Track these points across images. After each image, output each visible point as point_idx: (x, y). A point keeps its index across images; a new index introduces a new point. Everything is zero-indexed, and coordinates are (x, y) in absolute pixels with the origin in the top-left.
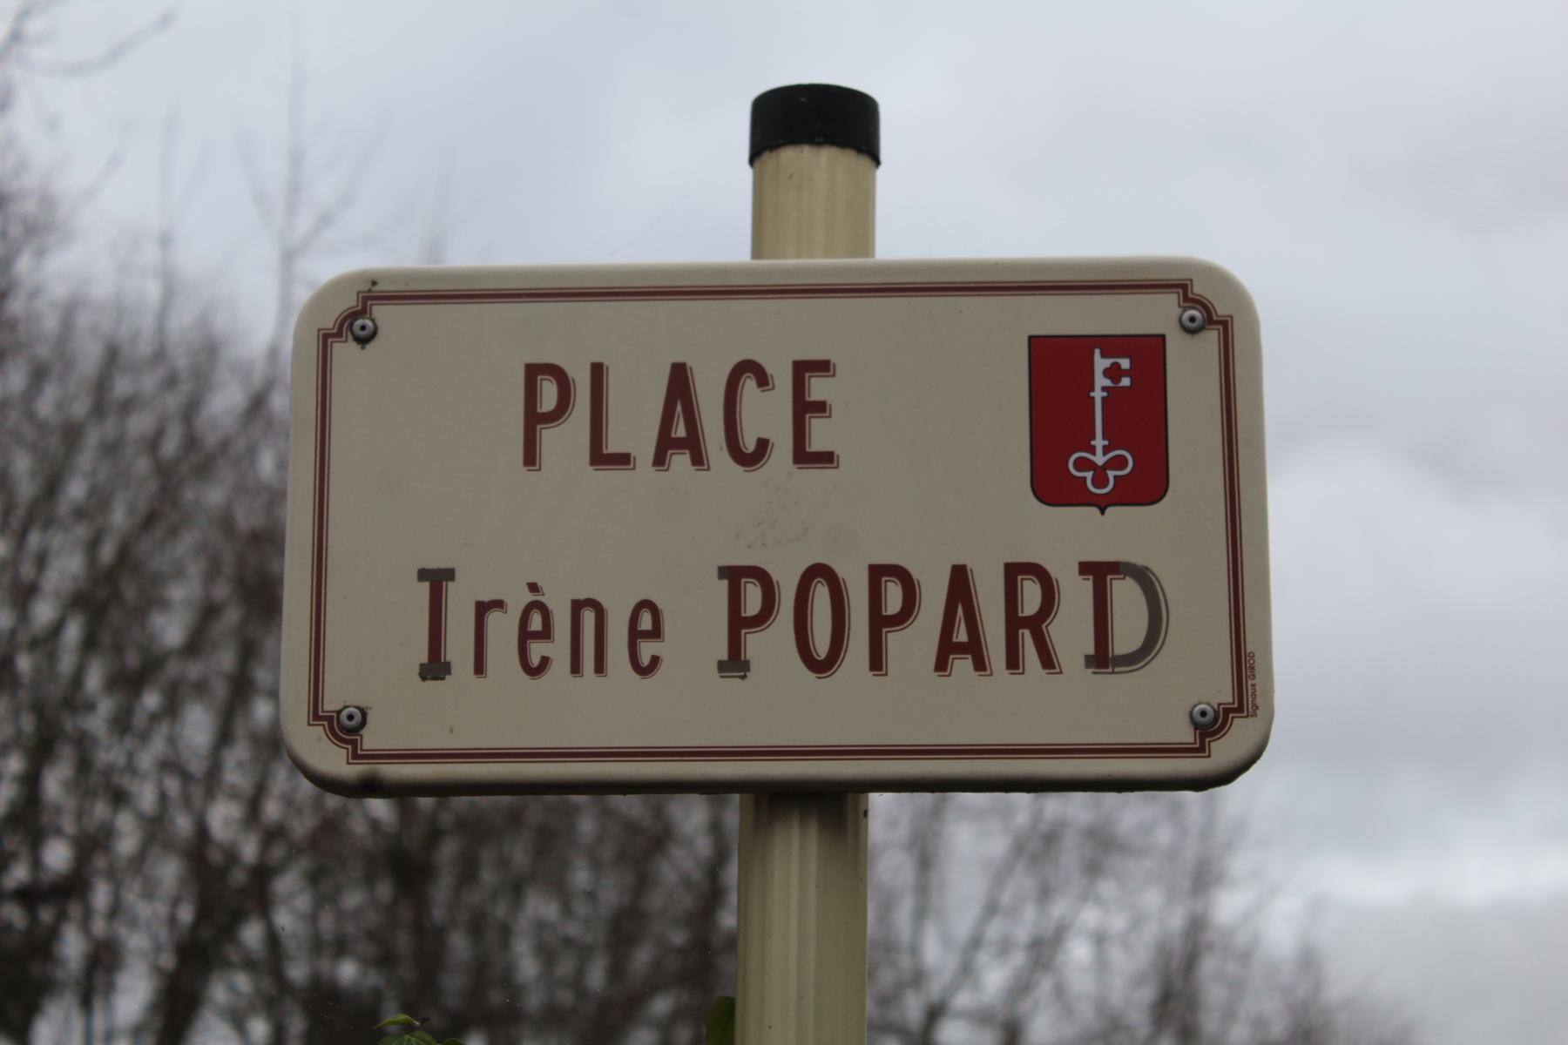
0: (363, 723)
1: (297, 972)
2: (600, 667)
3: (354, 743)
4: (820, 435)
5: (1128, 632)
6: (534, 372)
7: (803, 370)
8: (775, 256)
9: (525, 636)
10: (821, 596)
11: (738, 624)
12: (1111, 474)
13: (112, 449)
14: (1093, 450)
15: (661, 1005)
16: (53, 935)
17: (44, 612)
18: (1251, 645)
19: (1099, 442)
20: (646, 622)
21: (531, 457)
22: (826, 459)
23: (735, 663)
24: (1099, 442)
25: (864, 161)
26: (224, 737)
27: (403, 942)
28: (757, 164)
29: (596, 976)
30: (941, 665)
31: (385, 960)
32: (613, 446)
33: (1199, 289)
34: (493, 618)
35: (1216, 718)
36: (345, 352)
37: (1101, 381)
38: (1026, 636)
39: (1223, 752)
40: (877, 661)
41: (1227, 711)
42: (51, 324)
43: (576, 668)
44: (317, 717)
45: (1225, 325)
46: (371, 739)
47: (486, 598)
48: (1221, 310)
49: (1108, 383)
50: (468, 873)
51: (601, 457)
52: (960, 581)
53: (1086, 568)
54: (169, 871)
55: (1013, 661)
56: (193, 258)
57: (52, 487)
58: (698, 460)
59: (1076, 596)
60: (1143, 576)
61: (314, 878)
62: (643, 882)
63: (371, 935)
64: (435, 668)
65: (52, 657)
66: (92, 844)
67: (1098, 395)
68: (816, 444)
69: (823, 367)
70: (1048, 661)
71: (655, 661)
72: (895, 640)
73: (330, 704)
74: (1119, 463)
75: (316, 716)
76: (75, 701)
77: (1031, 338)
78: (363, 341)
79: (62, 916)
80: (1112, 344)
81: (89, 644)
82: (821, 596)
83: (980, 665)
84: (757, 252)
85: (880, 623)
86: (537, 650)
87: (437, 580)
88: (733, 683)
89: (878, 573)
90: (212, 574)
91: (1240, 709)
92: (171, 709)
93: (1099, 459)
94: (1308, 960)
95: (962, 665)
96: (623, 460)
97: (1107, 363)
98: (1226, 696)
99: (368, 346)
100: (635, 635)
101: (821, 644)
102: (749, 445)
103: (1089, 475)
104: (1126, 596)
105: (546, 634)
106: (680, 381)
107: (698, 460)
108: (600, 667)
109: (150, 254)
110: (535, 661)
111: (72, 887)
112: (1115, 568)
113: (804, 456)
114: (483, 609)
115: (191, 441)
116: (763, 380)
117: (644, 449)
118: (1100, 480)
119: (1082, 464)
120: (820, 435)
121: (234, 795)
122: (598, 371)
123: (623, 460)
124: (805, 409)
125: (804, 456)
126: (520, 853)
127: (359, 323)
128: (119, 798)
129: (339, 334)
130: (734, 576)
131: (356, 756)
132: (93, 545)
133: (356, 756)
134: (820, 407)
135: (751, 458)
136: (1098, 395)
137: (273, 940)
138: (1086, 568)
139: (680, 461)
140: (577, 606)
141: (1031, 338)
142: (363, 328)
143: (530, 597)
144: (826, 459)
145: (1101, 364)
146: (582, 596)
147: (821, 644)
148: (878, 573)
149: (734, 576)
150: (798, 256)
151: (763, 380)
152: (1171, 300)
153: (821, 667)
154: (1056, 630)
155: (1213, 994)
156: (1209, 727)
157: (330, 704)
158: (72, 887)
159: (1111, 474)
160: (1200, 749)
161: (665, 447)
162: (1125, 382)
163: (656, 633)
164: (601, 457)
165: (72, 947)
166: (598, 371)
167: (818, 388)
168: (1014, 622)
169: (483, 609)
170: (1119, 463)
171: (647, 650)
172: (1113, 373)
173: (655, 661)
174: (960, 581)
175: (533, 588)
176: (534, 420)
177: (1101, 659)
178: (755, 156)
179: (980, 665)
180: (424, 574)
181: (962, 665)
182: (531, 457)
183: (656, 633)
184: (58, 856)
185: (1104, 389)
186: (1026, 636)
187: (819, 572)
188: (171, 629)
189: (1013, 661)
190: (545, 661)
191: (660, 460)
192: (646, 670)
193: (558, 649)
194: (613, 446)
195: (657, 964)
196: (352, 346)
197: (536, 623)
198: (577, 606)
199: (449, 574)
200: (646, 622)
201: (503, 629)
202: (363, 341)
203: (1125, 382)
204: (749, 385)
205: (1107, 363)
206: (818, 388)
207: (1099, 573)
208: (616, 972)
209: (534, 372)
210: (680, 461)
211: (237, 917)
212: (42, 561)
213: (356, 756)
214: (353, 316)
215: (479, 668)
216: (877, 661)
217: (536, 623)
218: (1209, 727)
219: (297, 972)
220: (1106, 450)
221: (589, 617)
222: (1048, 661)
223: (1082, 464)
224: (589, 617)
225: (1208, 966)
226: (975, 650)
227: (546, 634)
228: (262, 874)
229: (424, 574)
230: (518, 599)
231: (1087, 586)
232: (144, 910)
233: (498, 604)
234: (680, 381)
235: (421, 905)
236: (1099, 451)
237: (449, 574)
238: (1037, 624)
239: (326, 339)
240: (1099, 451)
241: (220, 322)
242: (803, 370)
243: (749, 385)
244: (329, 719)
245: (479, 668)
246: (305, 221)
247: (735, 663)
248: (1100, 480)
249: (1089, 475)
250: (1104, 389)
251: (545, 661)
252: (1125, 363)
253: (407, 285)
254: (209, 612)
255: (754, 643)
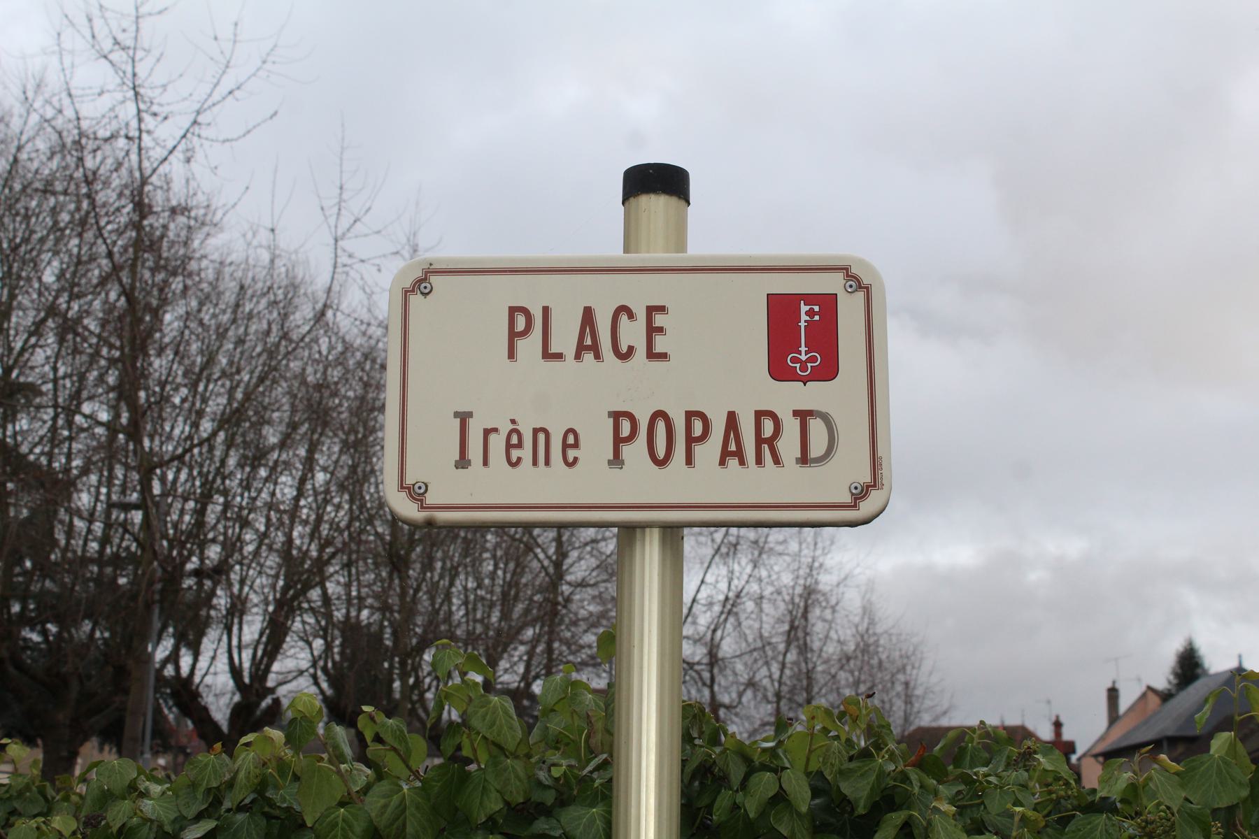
0: (426, 490)
1: (339, 615)
2: (547, 463)
3: (421, 501)
4: (660, 344)
5: (818, 446)
6: (513, 311)
7: (652, 310)
8: (637, 252)
9: (509, 446)
10: (661, 426)
11: (618, 441)
12: (809, 365)
13: (240, 342)
14: (800, 353)
15: (529, 633)
16: (213, 593)
17: (207, 426)
18: (880, 453)
19: (803, 349)
20: (571, 440)
21: (512, 355)
22: (663, 356)
23: (617, 460)
24: (803, 349)
25: (683, 203)
26: (300, 493)
27: (394, 600)
28: (627, 204)
29: (495, 617)
30: (722, 462)
31: (385, 608)
32: (554, 349)
33: (854, 271)
34: (492, 437)
35: (862, 490)
36: (415, 300)
37: (804, 317)
38: (766, 447)
39: (866, 507)
40: (689, 461)
41: (868, 487)
42: (210, 274)
43: (535, 463)
44: (402, 487)
45: (867, 289)
46: (430, 499)
47: (489, 427)
48: (866, 281)
49: (808, 318)
50: (428, 565)
51: (547, 355)
52: (732, 419)
53: (796, 413)
54: (272, 561)
55: (759, 461)
56: (286, 241)
57: (210, 361)
58: (598, 356)
59: (791, 427)
60: (825, 418)
61: (347, 566)
62: (520, 568)
63: (376, 596)
64: (463, 462)
65: (211, 449)
66: (232, 546)
67: (803, 324)
68: (658, 348)
69: (662, 309)
70: (777, 460)
71: (576, 459)
72: (698, 449)
73: (409, 481)
74: (813, 359)
75: (402, 487)
76: (220, 472)
77: (770, 297)
78: (425, 295)
79: (216, 584)
80: (809, 298)
81: (229, 444)
82: (661, 426)
83: (742, 462)
84: (626, 250)
85: (690, 440)
86: (515, 454)
87: (464, 418)
88: (616, 471)
89: (690, 415)
90: (294, 410)
91: (874, 486)
92: (272, 478)
93: (803, 357)
94: (867, 610)
95: (733, 462)
96: (559, 356)
97: (807, 308)
98: (867, 479)
99: (428, 297)
100: (565, 446)
101: (661, 452)
102: (624, 349)
103: (798, 365)
104: (817, 428)
105: (520, 445)
106: (588, 315)
107: (598, 356)
108: (547, 463)
109: (264, 237)
110: (514, 460)
111: (220, 571)
112: (810, 413)
113: (652, 355)
114: (487, 432)
115: (285, 336)
116: (631, 316)
117: (570, 351)
118: (804, 369)
119: (795, 360)
120: (660, 344)
121: (305, 523)
122: (546, 310)
123: (559, 356)
124: (653, 331)
125: (652, 355)
126: (455, 551)
127: (423, 285)
128: (245, 523)
129: (413, 291)
130: (617, 416)
131: (422, 507)
132: (231, 393)
133: (423, 507)
134: (660, 330)
135: (625, 355)
136: (803, 324)
137: (326, 599)
138: (796, 413)
139: (588, 357)
140: (536, 431)
141: (770, 297)
142: (425, 288)
143: (512, 427)
144: (663, 356)
145: (804, 308)
146: (538, 426)
147: (661, 452)
148: (690, 415)
149: (617, 416)
150: (648, 252)
151: (631, 316)
152: (840, 276)
153: (661, 463)
154: (781, 445)
155: (818, 628)
156: (860, 494)
157: (409, 481)
158: (220, 571)
159: (809, 365)
160: (854, 506)
161: (580, 350)
162: (817, 318)
163: (576, 445)
164: (547, 355)
165: (222, 600)
166: (546, 310)
167: (659, 320)
168: (759, 441)
169: (487, 432)
170: (813, 359)
171: (571, 454)
172: (810, 313)
173: (576, 459)
174: (732, 419)
175: (513, 422)
176: (513, 336)
177: (804, 459)
178: (623, 203)
179: (742, 462)
180: (456, 414)
181: (733, 462)
182: (512, 355)
183: (576, 445)
184: (214, 552)
185: (806, 321)
186: (766, 447)
187: (659, 414)
188: (272, 436)
189: (759, 461)
190: (519, 459)
191: (578, 356)
192: (571, 464)
193: (526, 453)
194: (554, 349)
195: (527, 611)
196: (419, 295)
197: (514, 440)
198: (536, 431)
199: (470, 414)
200: (571, 440)
201: (497, 443)
202: (425, 295)
203: (817, 318)
204: (624, 318)
205: (807, 308)
206: (659, 320)
207: (803, 416)
208: (505, 616)
209: (513, 311)
210: (588, 357)
211: (307, 587)
212: (205, 401)
213: (422, 507)
214: (420, 281)
215: (485, 463)
216: (689, 461)
217: (514, 440)
218: (860, 494)
219: (339, 615)
220: (807, 353)
221: (541, 437)
222: (777, 460)
223: (795, 360)
224: (541, 437)
225: (816, 612)
226: (740, 455)
227: (520, 445)
228: (321, 564)
229: (456, 414)
230: (505, 428)
231: (796, 423)
232: (261, 581)
233: (495, 430)
234: (588, 315)
235: (404, 578)
236: (803, 353)
237: (470, 414)
238: (771, 442)
239: (406, 293)
240: (803, 353)
241: (300, 273)
242: (652, 310)
243: (624, 318)
244: (409, 488)
245: (485, 463)
246: (345, 222)
247: (617, 460)
248: (804, 369)
249: (798, 365)
250: (806, 321)
251: (519, 459)
252: (816, 308)
253: (328, 245)
254: (293, 426)
255: (626, 450)
